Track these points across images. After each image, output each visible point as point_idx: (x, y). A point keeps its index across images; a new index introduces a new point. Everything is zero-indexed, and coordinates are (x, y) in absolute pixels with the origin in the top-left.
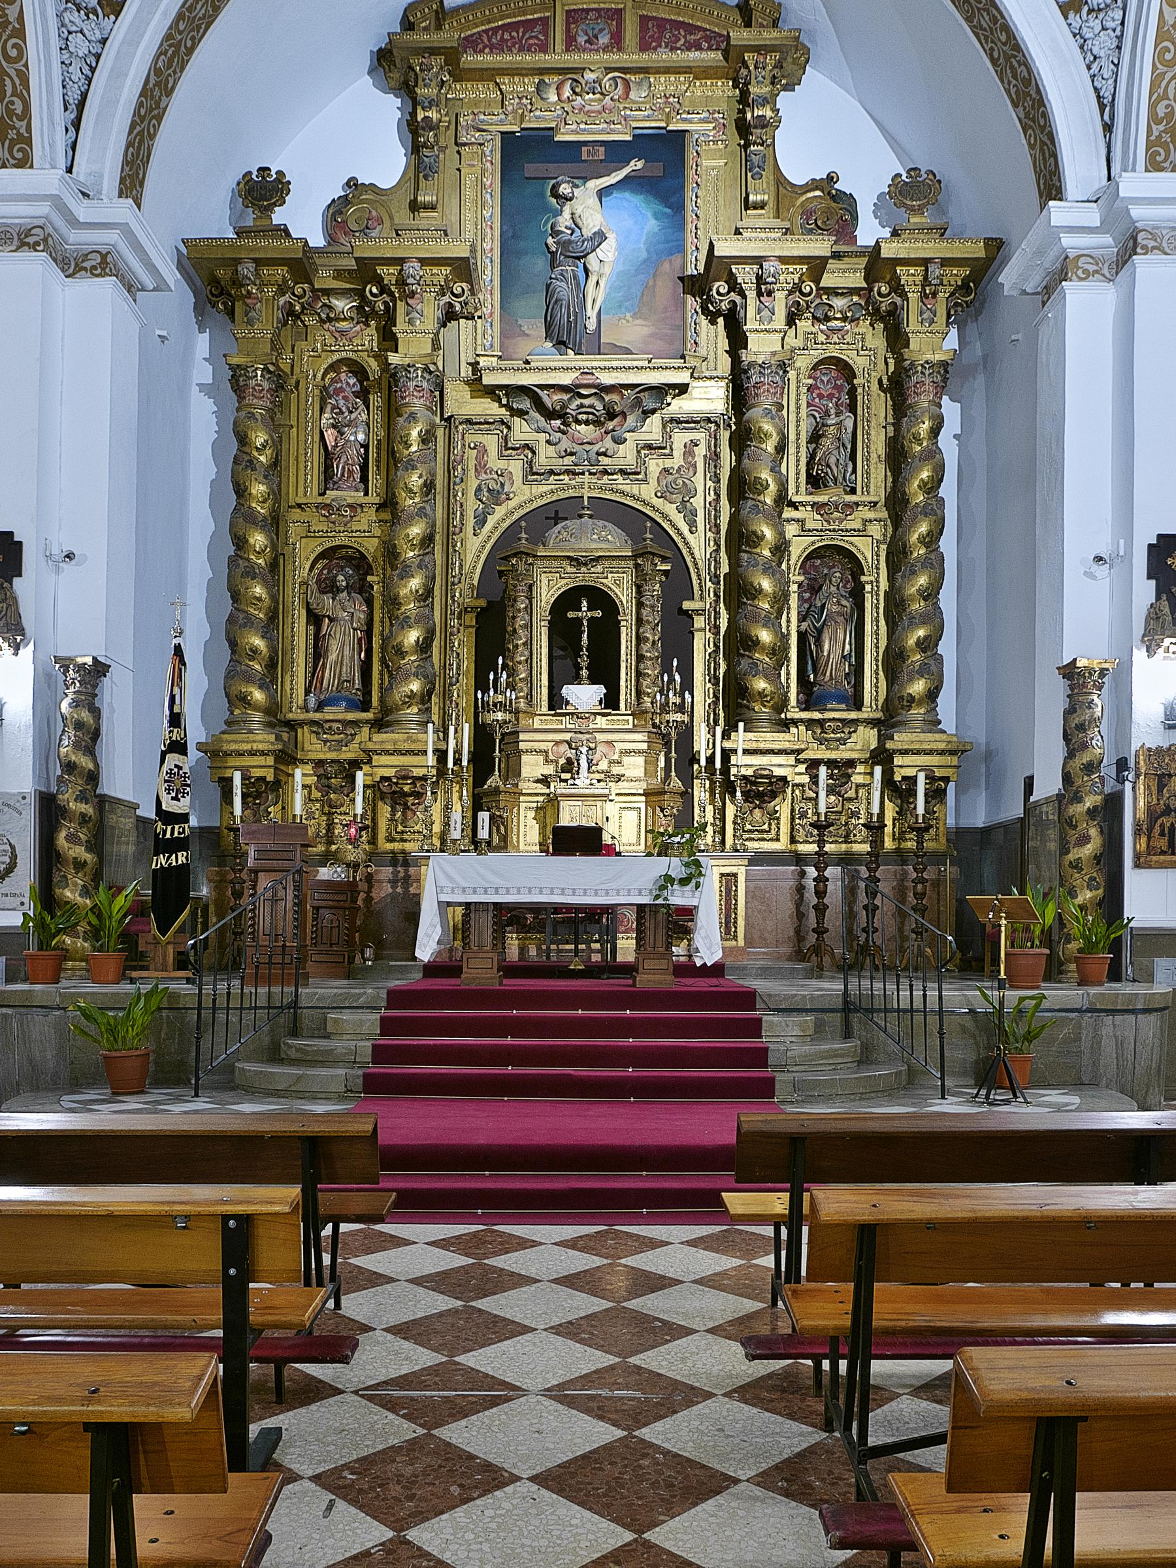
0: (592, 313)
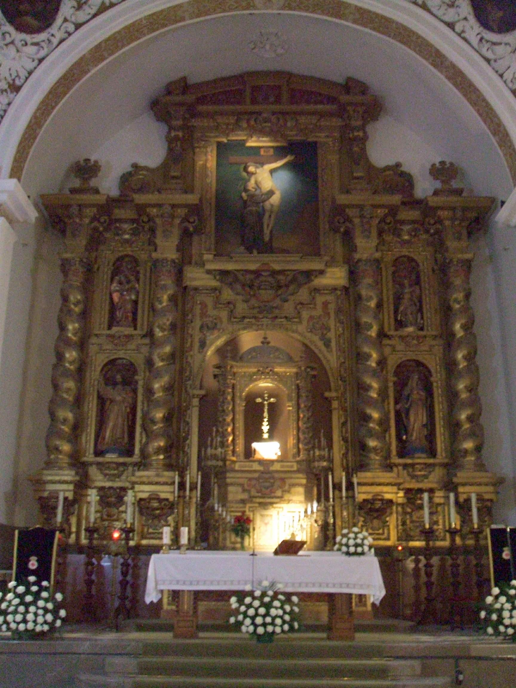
0: (267, 232)
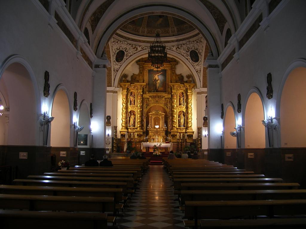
0: (157, 87)
